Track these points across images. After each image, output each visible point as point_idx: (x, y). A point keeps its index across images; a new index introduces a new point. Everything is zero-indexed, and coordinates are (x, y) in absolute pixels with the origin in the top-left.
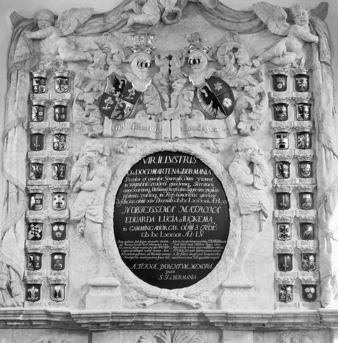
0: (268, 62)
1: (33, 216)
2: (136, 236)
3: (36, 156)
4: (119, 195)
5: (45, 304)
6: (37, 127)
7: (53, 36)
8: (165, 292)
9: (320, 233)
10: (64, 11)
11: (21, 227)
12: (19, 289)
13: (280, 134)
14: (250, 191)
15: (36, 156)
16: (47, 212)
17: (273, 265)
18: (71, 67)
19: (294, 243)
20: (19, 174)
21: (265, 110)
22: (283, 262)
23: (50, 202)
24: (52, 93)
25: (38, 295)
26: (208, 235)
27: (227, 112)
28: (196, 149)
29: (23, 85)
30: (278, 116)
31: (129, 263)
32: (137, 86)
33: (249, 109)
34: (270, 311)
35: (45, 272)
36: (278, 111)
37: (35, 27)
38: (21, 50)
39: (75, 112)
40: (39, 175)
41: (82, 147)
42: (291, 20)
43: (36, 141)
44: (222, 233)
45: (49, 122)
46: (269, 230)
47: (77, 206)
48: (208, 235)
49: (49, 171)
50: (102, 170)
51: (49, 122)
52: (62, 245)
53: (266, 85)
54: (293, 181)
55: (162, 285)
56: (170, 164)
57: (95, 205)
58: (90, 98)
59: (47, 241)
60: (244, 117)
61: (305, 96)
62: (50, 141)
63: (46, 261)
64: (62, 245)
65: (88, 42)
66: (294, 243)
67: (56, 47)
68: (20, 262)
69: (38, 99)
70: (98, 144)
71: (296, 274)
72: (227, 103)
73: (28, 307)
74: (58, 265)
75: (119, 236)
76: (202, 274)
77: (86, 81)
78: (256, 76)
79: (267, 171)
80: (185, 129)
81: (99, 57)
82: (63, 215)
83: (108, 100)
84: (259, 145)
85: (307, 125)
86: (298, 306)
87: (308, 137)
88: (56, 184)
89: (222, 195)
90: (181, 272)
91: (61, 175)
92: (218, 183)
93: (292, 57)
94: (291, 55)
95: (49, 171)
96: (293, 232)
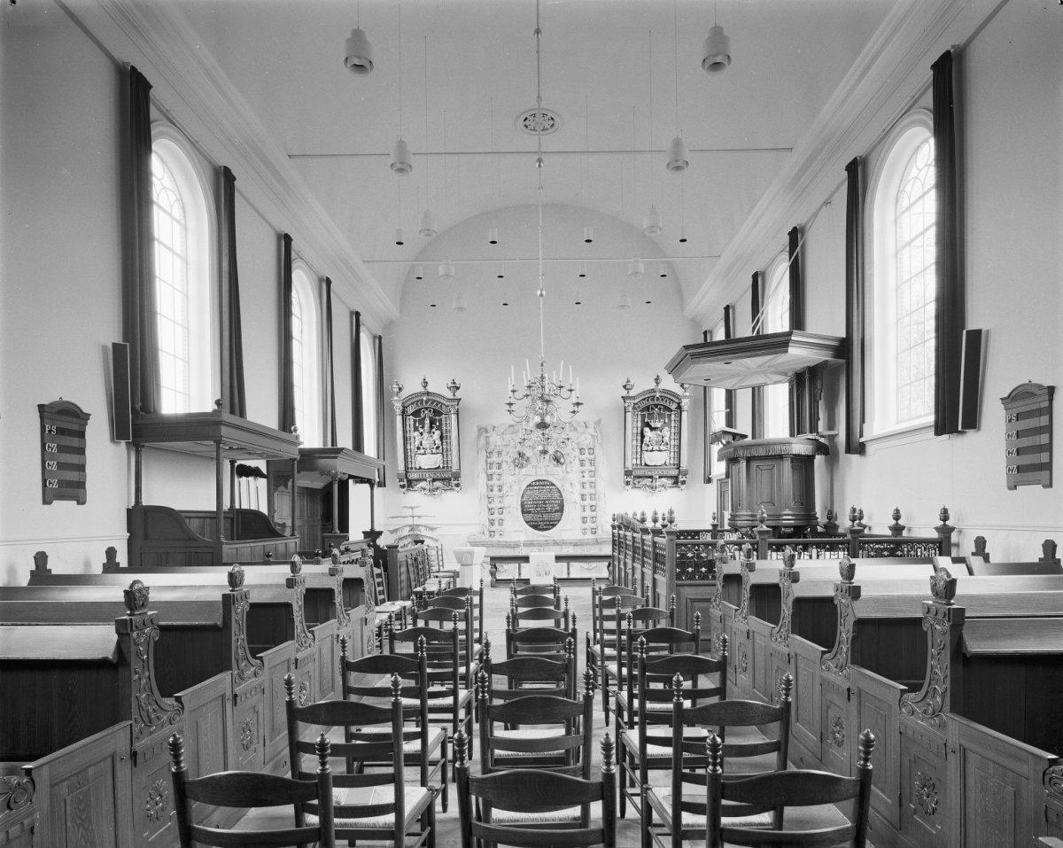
0: (578, 443)
1: (490, 506)
2: (529, 512)
3: (492, 517)
4: (522, 497)
5: (497, 538)
6: (490, 472)
7: (494, 435)
8: (541, 533)
9: (597, 509)
10: (510, 602)
11: (486, 510)
12: (487, 533)
13: (584, 483)
14: (572, 497)
15: (490, 483)
16: (496, 505)
17: (580, 521)
18: (502, 447)
19: (588, 513)
20: (484, 490)
21: (577, 462)
22: (584, 520)
23: (497, 500)
24: (495, 458)
25: (494, 535)
26: (556, 511)
27: (562, 464)
28: (551, 479)
29: (483, 455)
30: (582, 465)
31: (527, 522)
32: (527, 455)
33: (571, 463)
34: (579, 538)
35: (496, 516)
36: (582, 463)
37: (487, 432)
38: (482, 441)
39: (504, 465)
40: (492, 490)
41: (508, 479)
42: (586, 427)
43: (490, 477)
44: (561, 510)
45: (494, 470)
46: (580, 509)
47: (506, 502)
48: (556, 511)
49: (496, 489)
50: (516, 488)
51: (494, 470)
52: (502, 516)
53: (577, 452)
54: (588, 490)
55: (540, 530)
56: (541, 483)
57: (513, 502)
58: (510, 460)
59: (496, 515)
60: (569, 465)
61: (592, 457)
62: (495, 477)
63: (496, 523)
64: (502, 516)
65: (508, 437)
66: (588, 513)
67: (496, 440)
68: (487, 523)
69: (489, 461)
70: (513, 478)
71: (589, 525)
72: (562, 460)
73: (491, 539)
74: (500, 524)
75: (523, 512)
76: (554, 526)
77: (508, 453)
78: (573, 449)
79: (578, 486)
80: (546, 471)
81: (512, 444)
82: (502, 505)
83: (517, 461)
84: (575, 477)
85: (593, 468)
86: (589, 536)
87: (593, 473)
88: (498, 494)
89: (561, 496)
90: (546, 525)
91: (500, 490)
92: (559, 491)
93: (587, 442)
94: (586, 441)
95: (496, 489)
96: (587, 509)
